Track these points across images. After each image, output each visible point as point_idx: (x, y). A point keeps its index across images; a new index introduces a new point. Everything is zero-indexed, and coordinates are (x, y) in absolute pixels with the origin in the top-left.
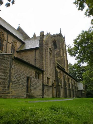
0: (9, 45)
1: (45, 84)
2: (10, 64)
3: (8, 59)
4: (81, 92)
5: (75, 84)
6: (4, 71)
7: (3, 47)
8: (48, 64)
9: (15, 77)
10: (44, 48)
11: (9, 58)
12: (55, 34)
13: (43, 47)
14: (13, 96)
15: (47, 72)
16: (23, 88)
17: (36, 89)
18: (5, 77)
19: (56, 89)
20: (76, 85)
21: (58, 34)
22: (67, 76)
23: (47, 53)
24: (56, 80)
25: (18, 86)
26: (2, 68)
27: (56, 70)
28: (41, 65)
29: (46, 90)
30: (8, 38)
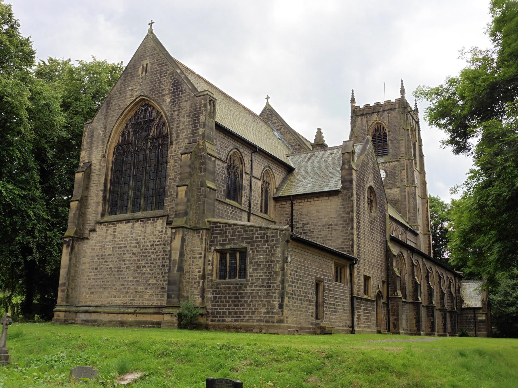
0: (256, 183)
1: (358, 294)
2: (283, 254)
3: (277, 240)
4: (473, 315)
5: (449, 287)
7: (243, 191)
8: (364, 237)
9: (293, 282)
10: (354, 192)
11: (279, 237)
12: (382, 102)
13: (352, 189)
14: (289, 327)
16: (309, 309)
17: (335, 308)
18: (271, 283)
19: (388, 307)
20: (453, 291)
21: (394, 103)
22: (424, 264)
23: (362, 204)
24: (388, 280)
25: (299, 303)
26: (262, 262)
27: (388, 253)
28: (347, 242)
29: (361, 312)
30: (254, 164)
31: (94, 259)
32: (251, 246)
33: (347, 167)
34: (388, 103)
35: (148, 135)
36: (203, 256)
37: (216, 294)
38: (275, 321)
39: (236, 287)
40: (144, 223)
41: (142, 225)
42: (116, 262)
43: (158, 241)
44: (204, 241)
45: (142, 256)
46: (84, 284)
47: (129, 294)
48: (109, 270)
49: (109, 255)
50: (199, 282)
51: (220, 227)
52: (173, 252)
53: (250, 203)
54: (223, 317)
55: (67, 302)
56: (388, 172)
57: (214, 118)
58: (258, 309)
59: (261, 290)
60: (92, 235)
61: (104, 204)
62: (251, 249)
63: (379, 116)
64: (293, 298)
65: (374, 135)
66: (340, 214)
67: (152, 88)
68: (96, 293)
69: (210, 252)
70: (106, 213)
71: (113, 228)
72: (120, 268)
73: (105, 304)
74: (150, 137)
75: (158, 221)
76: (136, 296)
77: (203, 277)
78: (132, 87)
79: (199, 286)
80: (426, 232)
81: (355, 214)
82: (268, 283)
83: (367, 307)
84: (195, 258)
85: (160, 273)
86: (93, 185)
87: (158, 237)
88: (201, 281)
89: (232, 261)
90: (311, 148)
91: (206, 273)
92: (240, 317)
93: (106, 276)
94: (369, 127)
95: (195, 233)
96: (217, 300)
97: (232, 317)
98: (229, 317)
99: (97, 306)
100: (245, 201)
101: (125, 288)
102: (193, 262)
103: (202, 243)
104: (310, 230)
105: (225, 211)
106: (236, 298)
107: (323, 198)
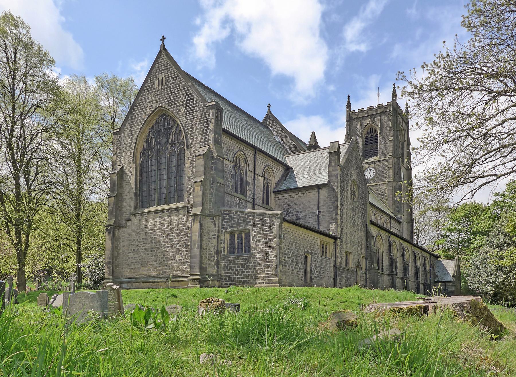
0: (259, 179)
5: (424, 264)
12: (375, 106)
15: (344, 240)
27: (367, 233)
31: (132, 242)
34: (380, 106)
35: (168, 141)
36: (216, 236)
37: (228, 265)
39: (243, 259)
40: (170, 213)
41: (167, 214)
42: (149, 244)
43: (181, 227)
44: (217, 225)
46: (125, 262)
48: (144, 250)
49: (143, 239)
50: (214, 256)
51: (229, 214)
52: (193, 234)
53: (254, 196)
54: (234, 281)
55: (113, 276)
56: (378, 170)
57: (221, 125)
60: (129, 223)
61: (136, 200)
62: (254, 230)
64: (286, 266)
66: (327, 203)
68: (135, 268)
69: (222, 233)
70: (138, 206)
71: (145, 217)
73: (143, 276)
74: (170, 142)
75: (180, 211)
76: (167, 269)
77: (217, 253)
79: (214, 259)
80: (409, 221)
81: (339, 203)
82: (267, 255)
83: (348, 275)
86: (125, 184)
88: (216, 255)
90: (306, 149)
91: (220, 250)
92: (246, 281)
93: (142, 255)
96: (229, 269)
97: (240, 281)
98: (238, 281)
99: (136, 278)
100: (250, 195)
101: (157, 264)
102: (209, 241)
103: (215, 227)
104: (303, 217)
105: (233, 202)
106: (243, 267)
107: (313, 191)
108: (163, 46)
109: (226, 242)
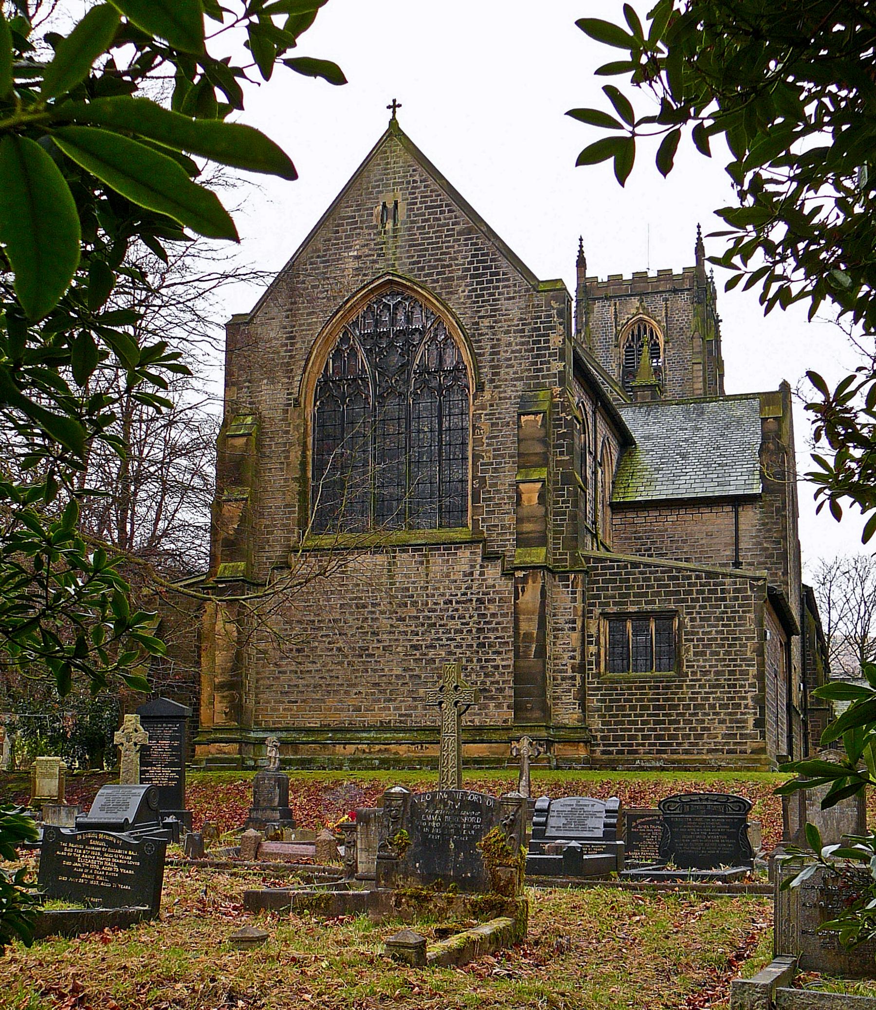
6: (728, 653)
32: (688, 607)
33: (771, 446)
34: (665, 275)
35: (409, 363)
36: (579, 624)
38: (749, 751)
41: (417, 558)
44: (578, 596)
45: (423, 625)
47: (396, 704)
48: (335, 652)
50: (573, 678)
58: (709, 729)
59: (716, 693)
62: (688, 613)
63: (644, 304)
65: (630, 346)
67: (415, 259)
72: (367, 650)
77: (581, 668)
78: (357, 250)
79: (574, 685)
84: (563, 630)
85: (475, 660)
87: (464, 586)
88: (578, 676)
89: (637, 635)
92: (671, 745)
94: (619, 328)
95: (557, 579)
97: (650, 745)
103: (574, 600)
108: (393, 123)
109: (602, 641)
